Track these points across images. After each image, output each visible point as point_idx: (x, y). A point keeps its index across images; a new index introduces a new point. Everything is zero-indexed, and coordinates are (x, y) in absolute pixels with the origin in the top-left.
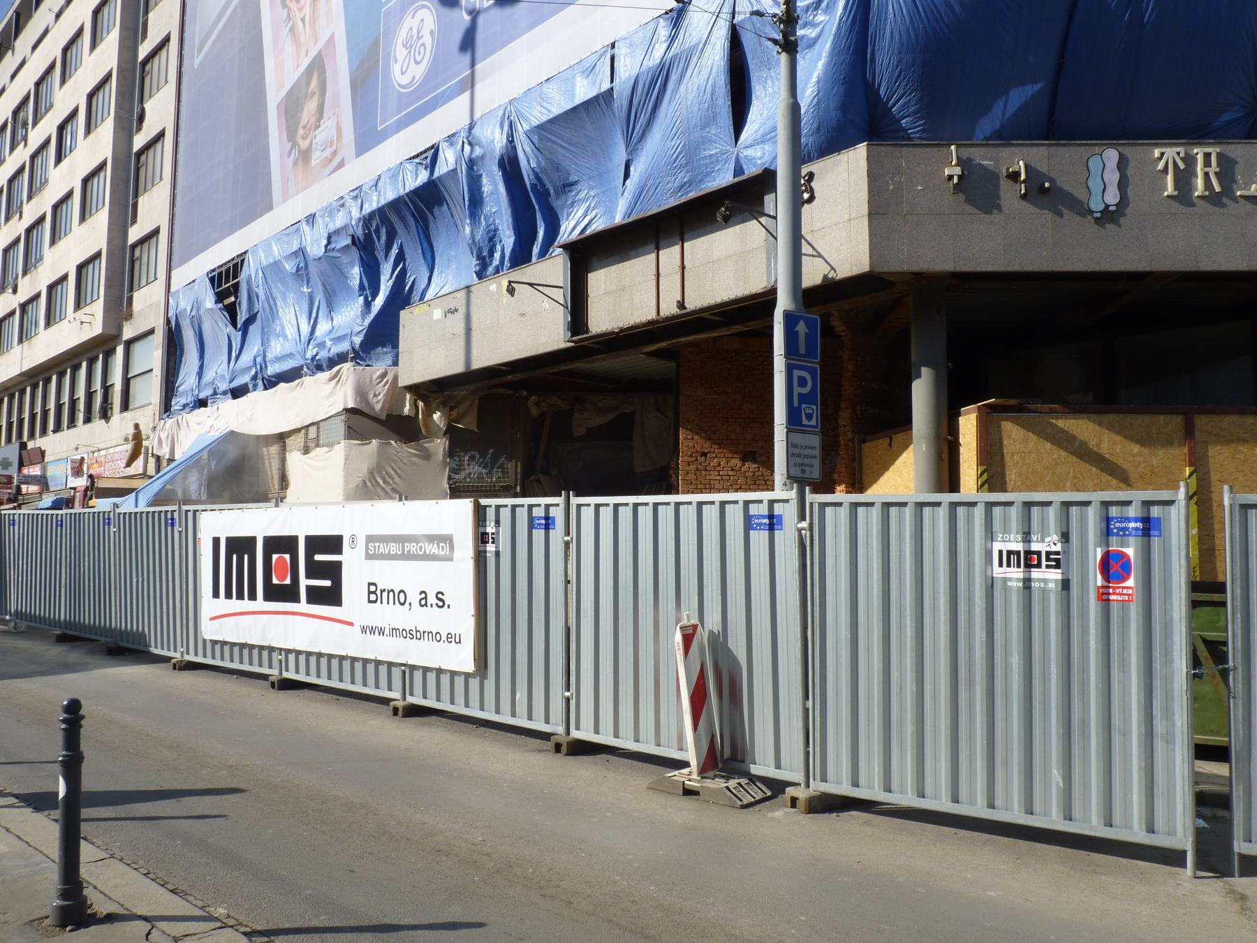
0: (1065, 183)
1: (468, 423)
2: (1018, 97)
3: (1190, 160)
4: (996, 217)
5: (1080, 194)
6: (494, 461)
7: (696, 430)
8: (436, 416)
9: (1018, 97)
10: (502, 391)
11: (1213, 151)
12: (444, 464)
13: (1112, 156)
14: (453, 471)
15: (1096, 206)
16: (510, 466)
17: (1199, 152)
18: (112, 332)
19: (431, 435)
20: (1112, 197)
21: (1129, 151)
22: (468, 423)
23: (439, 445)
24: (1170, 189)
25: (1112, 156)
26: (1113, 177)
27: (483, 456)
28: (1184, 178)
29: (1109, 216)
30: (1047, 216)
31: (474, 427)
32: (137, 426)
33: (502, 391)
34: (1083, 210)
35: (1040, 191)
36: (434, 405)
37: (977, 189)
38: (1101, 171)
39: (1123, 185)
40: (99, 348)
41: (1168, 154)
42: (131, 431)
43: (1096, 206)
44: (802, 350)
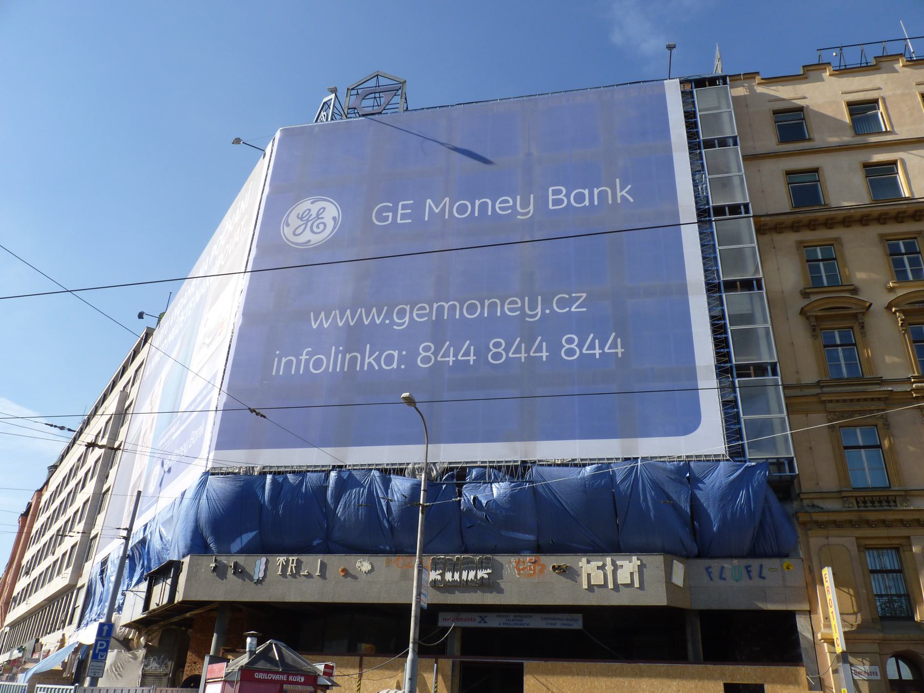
0: (248, 569)
1: (154, 643)
2: (247, 537)
3: (287, 561)
4: (225, 581)
5: (252, 573)
6: (163, 661)
7: (193, 653)
8: (142, 639)
9: (247, 537)
10: (173, 627)
11: (295, 558)
12: (142, 662)
13: (264, 559)
14: (146, 666)
15: (256, 578)
16: (169, 663)
17: (291, 558)
18: (73, 583)
19: (138, 647)
20: (261, 575)
21: (270, 558)
22: (154, 643)
23: (141, 653)
24: (279, 573)
25: (264, 559)
26: (263, 567)
27: (159, 659)
28: (285, 568)
29: (259, 582)
30: (240, 581)
31: (156, 645)
32: (63, 635)
33: (173, 627)
34: (251, 578)
35: (239, 571)
36: (143, 633)
37: (219, 570)
38: (259, 565)
39: (265, 570)
40: (69, 590)
41: (281, 559)
42: (61, 637)
43: (256, 578)
44: (104, 634)
